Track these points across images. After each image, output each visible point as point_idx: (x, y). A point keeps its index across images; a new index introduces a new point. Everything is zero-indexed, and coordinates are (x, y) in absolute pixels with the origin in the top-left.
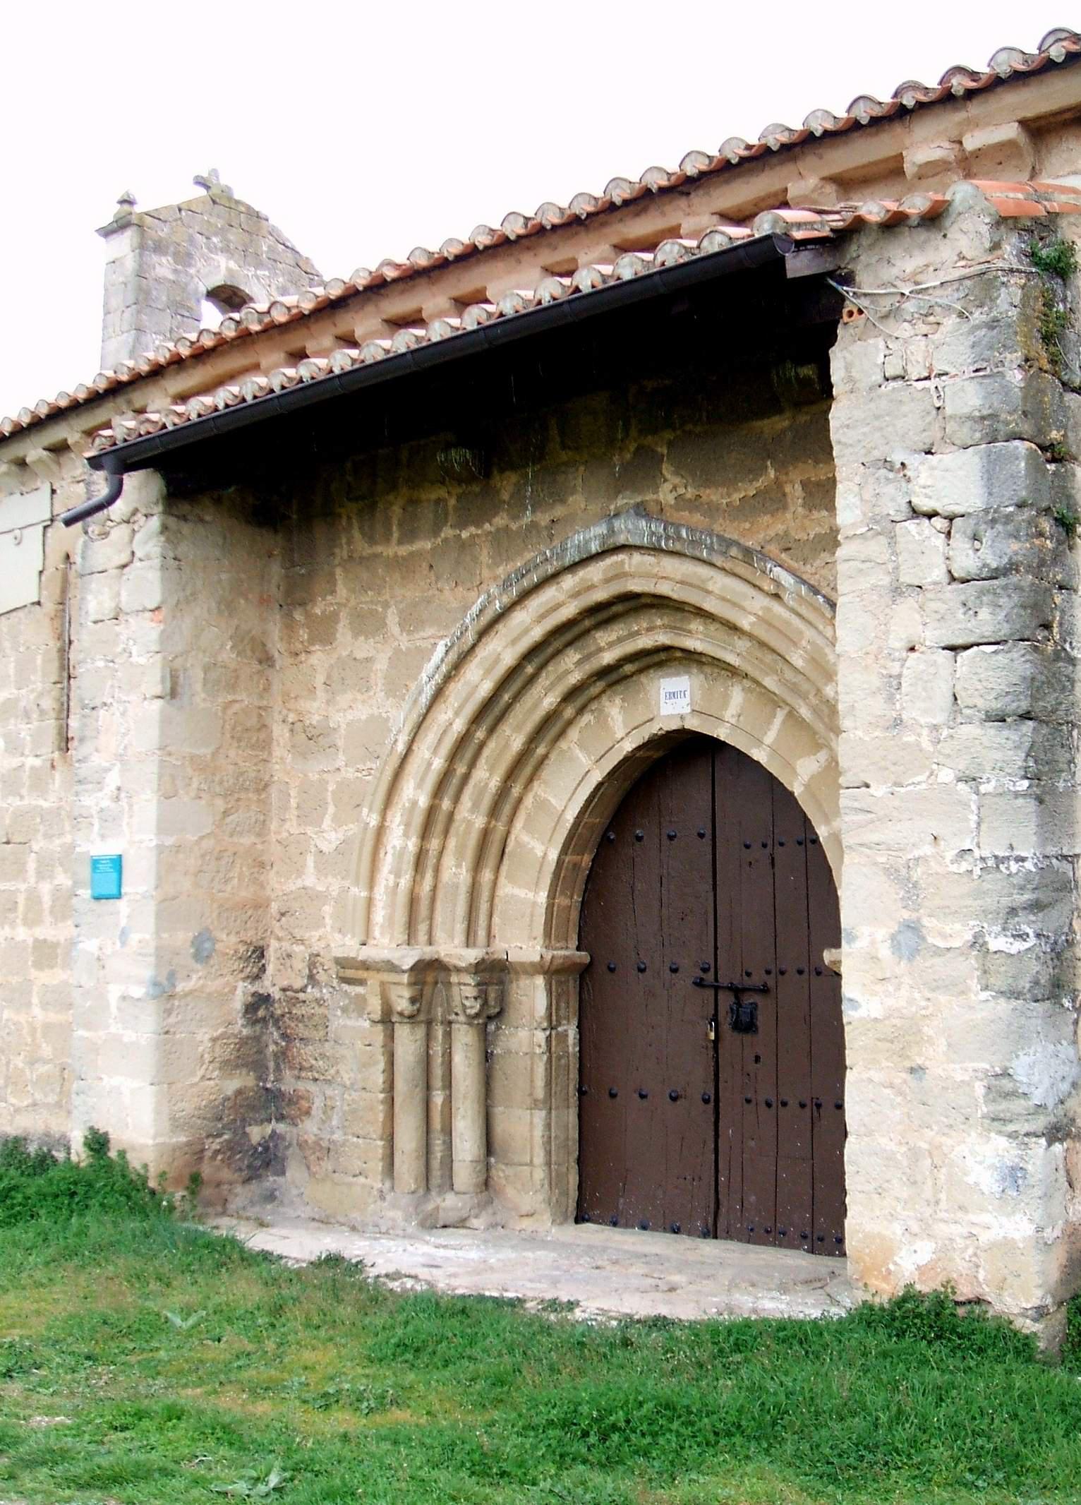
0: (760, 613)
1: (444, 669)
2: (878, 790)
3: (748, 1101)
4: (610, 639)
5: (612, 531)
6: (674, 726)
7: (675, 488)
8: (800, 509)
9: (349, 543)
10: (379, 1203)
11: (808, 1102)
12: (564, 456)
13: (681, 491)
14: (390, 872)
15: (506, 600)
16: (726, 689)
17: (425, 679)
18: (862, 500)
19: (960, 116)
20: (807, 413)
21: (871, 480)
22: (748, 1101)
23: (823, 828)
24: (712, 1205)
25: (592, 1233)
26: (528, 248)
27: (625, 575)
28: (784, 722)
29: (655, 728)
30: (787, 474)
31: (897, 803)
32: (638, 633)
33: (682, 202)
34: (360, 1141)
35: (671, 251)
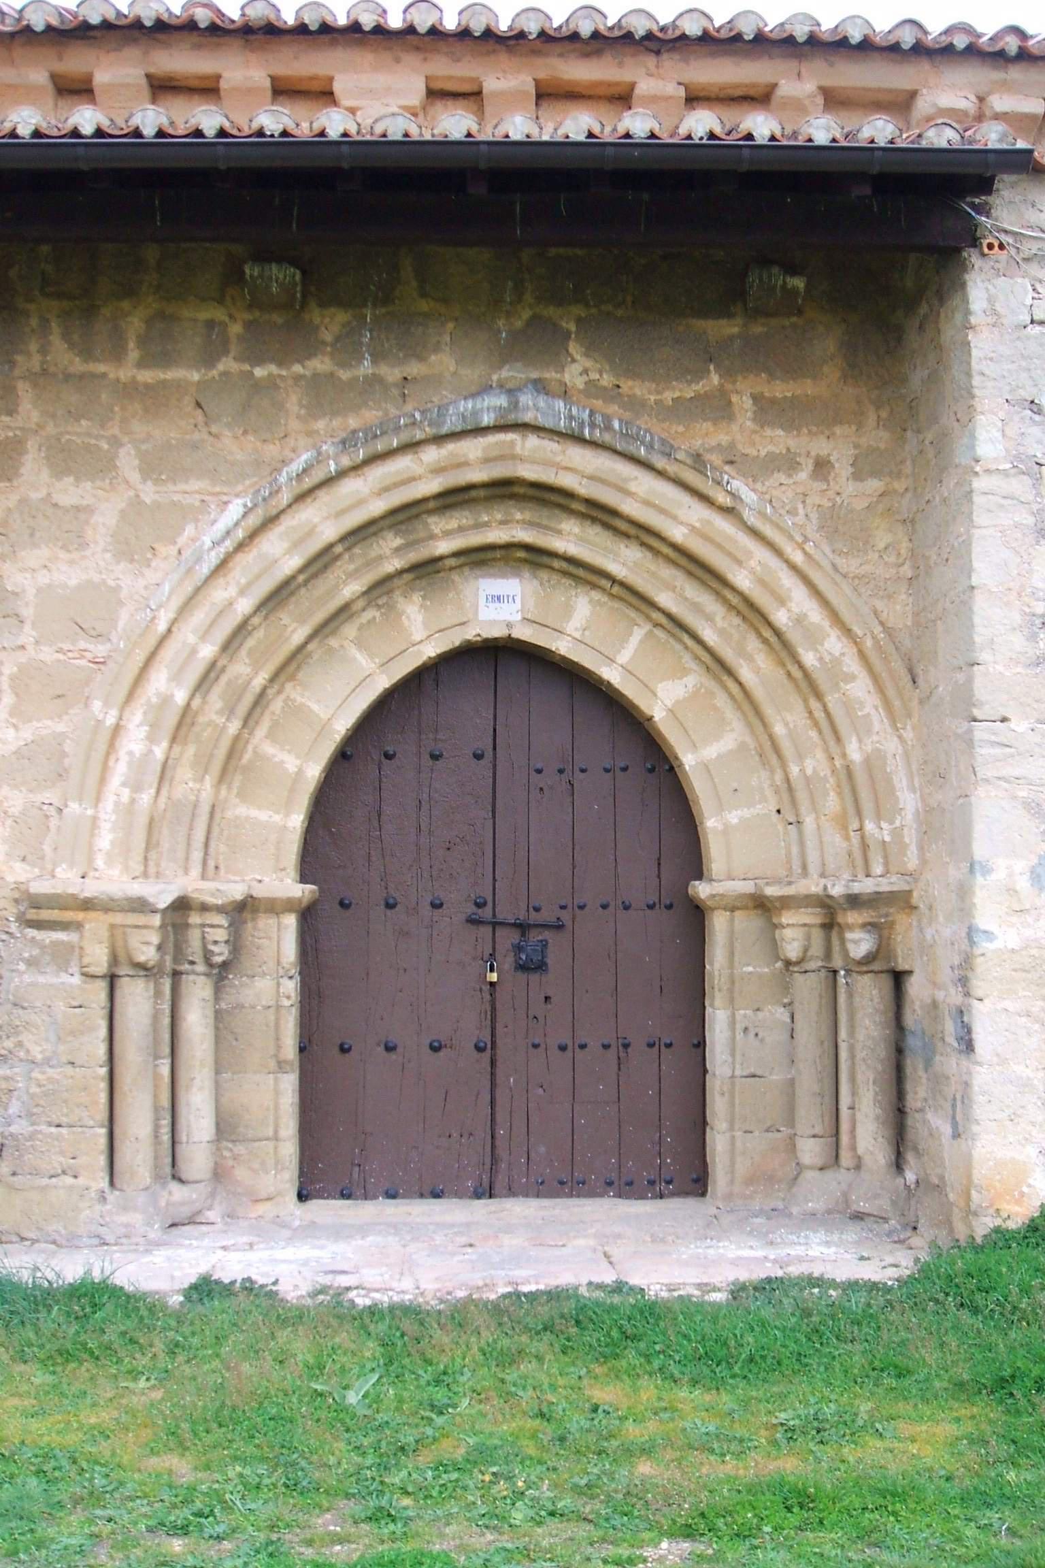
0: (697, 525)
1: (240, 534)
2: (1020, 725)
3: (536, 1046)
4: (449, 527)
5: (515, 405)
6: (497, 632)
7: (586, 371)
8: (749, 423)
9: (43, 351)
10: (98, 1207)
11: (613, 1043)
12: (424, 306)
13: (596, 376)
14: (124, 784)
15: (346, 462)
16: (569, 599)
17: (208, 544)
18: (1004, 435)
19: (997, 75)
20: (763, 325)
21: (1016, 418)
22: (536, 1046)
23: (690, 756)
24: (488, 1160)
25: (324, 1210)
26: (417, 49)
27: (514, 457)
28: (641, 641)
29: (470, 634)
30: (734, 382)
31: (1038, 739)
32: (486, 525)
33: (651, 61)
34: (64, 1131)
35: (884, 129)
